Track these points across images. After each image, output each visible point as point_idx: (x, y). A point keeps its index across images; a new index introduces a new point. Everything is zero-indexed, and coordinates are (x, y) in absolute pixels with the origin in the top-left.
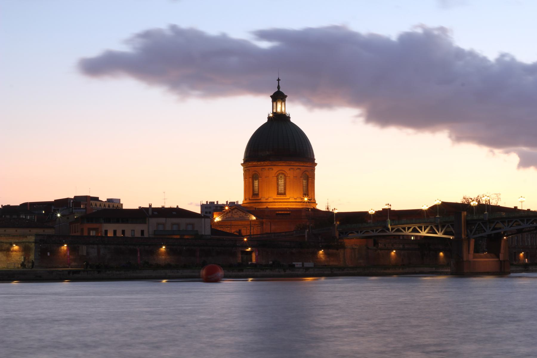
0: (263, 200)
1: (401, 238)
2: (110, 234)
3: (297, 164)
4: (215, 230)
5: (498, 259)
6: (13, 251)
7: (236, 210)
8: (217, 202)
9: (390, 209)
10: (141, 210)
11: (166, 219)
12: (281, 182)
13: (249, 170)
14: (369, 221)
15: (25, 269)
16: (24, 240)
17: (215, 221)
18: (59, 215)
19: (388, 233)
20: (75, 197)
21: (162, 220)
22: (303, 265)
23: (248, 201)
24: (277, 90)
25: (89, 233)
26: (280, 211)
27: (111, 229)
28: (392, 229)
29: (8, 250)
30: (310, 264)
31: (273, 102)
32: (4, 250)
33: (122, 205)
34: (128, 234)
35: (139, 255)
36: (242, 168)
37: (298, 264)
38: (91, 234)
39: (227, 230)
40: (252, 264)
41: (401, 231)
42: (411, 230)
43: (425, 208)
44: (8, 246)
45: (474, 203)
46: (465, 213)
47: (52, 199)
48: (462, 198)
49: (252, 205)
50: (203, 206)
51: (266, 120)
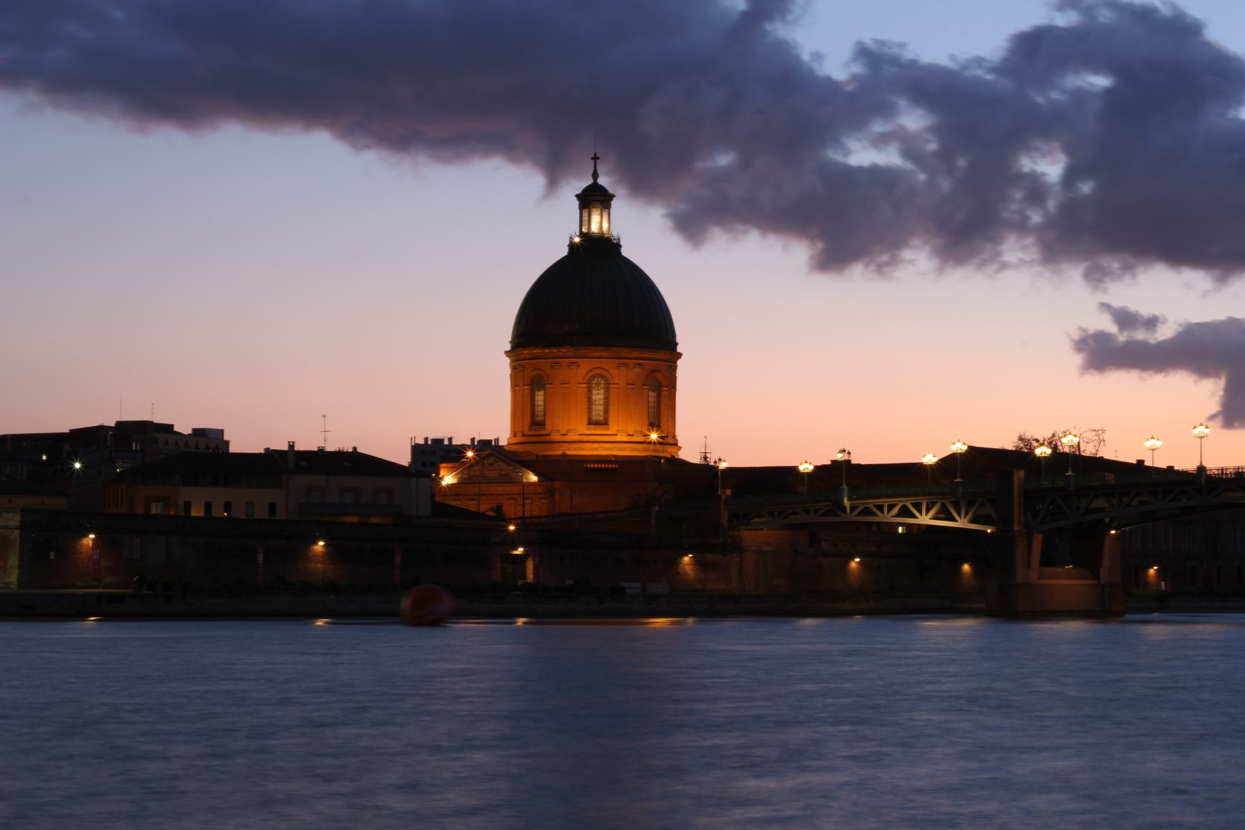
1: (875, 529)
2: (197, 512)
4: (442, 505)
5: (1095, 582)
7: (491, 460)
9: (848, 462)
10: (270, 455)
12: (598, 395)
13: (523, 366)
17: (444, 483)
19: (842, 518)
20: (118, 423)
21: (318, 480)
23: (519, 439)
24: (590, 181)
27: (197, 501)
28: (853, 508)
33: (227, 443)
34: (239, 512)
36: (507, 361)
37: (633, 587)
38: (153, 511)
39: (471, 506)
40: (526, 586)
41: (875, 515)
42: (895, 511)
43: (930, 459)
45: (1043, 451)
46: (1022, 474)
47: (64, 428)
48: (1016, 439)
49: (529, 448)
50: (416, 449)
51: (564, 252)
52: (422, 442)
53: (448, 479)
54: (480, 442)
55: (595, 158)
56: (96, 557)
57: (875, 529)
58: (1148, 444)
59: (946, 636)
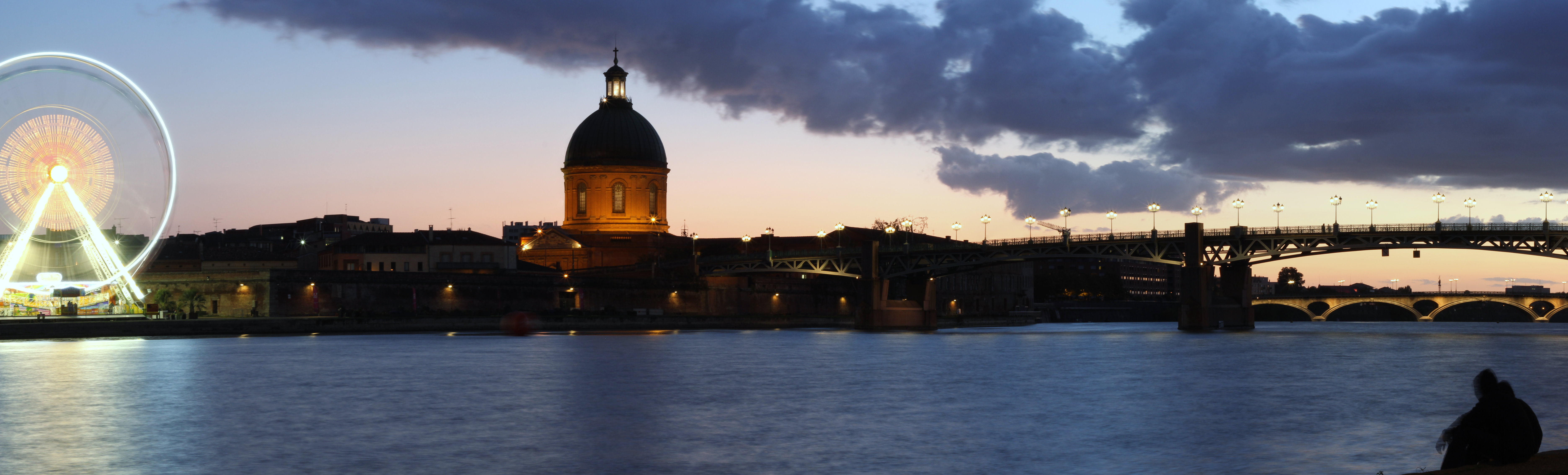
0: (593, 220)
1: (787, 276)
2: (375, 268)
3: (642, 170)
4: (524, 263)
5: (920, 309)
6: (241, 293)
7: (553, 235)
8: (527, 223)
9: (772, 235)
10: (419, 234)
11: (452, 249)
12: (619, 195)
13: (572, 177)
14: (743, 252)
15: (257, 318)
16: (256, 277)
17: (524, 249)
18: (303, 242)
19: (768, 269)
20: (326, 217)
21: (448, 248)
22: (648, 312)
23: (570, 222)
24: (613, 65)
25: (345, 267)
26: (617, 235)
27: (375, 262)
28: (775, 264)
29: (234, 292)
30: (658, 312)
31: (608, 81)
32: (228, 292)
33: (391, 227)
34: (400, 268)
35: (414, 297)
36: (562, 175)
37: (641, 311)
38: (349, 269)
39: (540, 262)
40: (575, 311)
41: (787, 267)
42: (801, 265)
43: (822, 234)
44: (233, 285)
45: (890, 230)
46: (877, 243)
47: (293, 220)
48: (874, 222)
49: (577, 227)
50: (506, 229)
51: (597, 108)
52: (509, 224)
53: (526, 247)
54: (545, 224)
55: (616, 51)
56: (316, 297)
57: (787, 276)
58: (953, 227)
59: (830, 342)
